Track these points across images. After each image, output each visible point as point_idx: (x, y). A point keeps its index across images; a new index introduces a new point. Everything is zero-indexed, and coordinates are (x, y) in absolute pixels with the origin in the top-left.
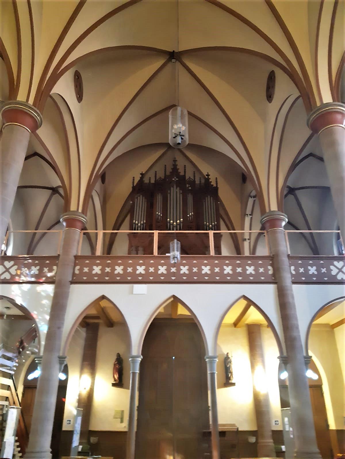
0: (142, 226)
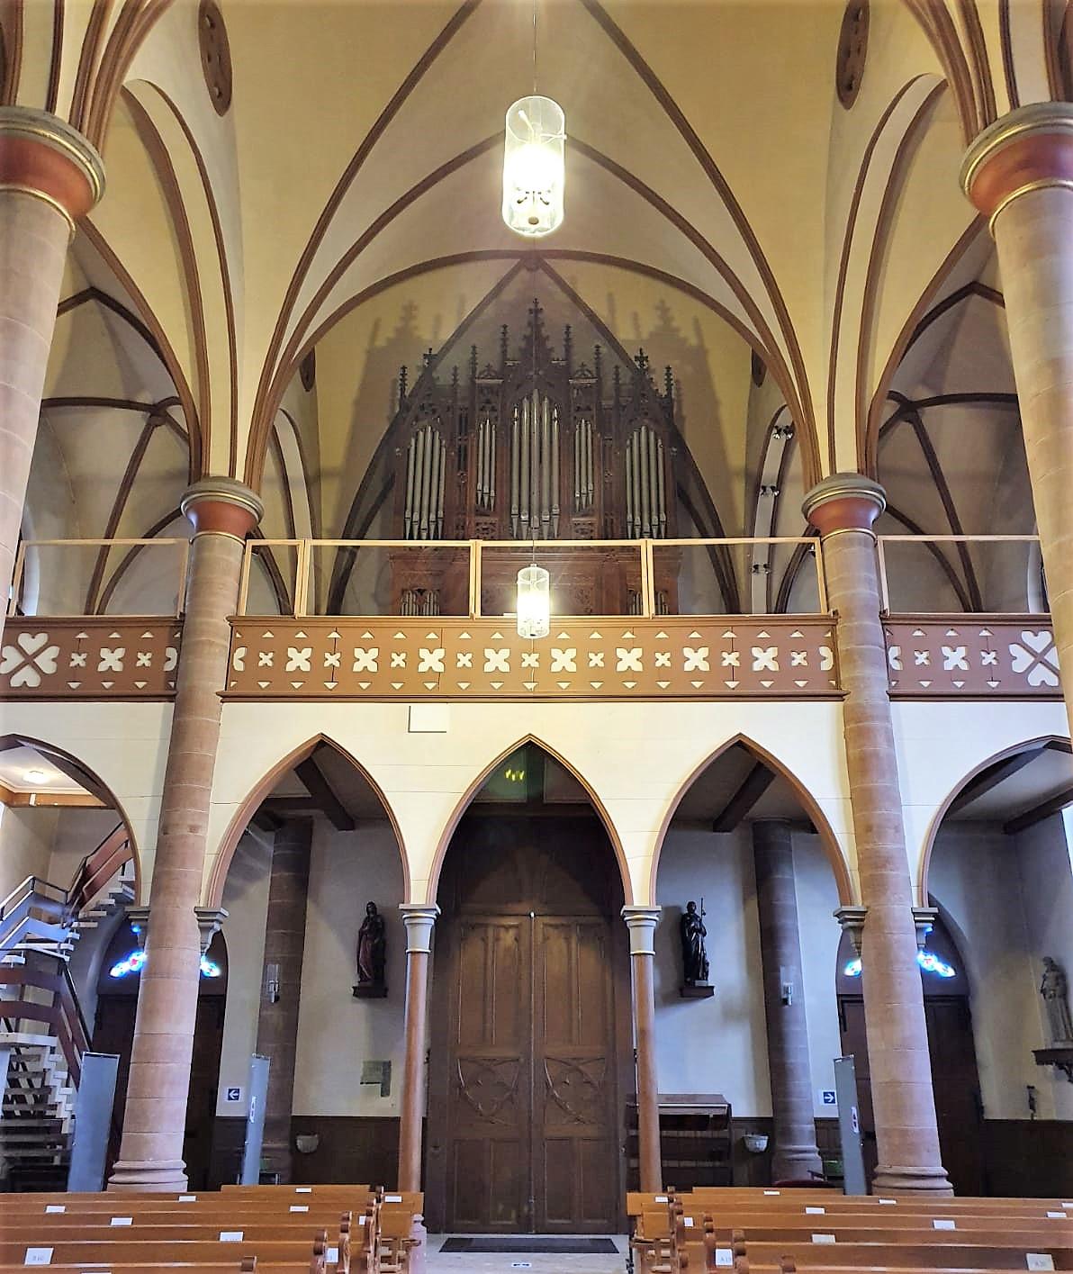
0: (432, 527)
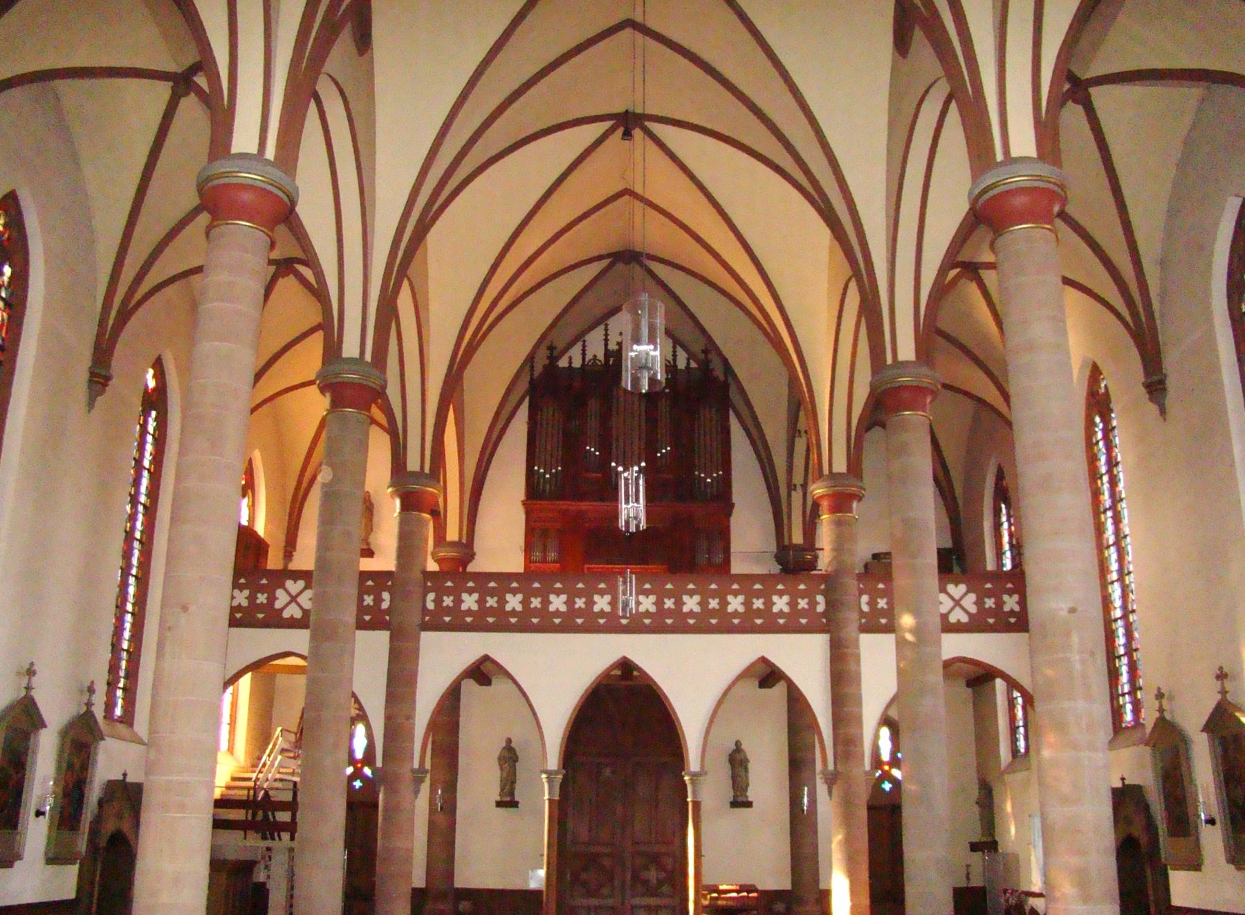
0: (554, 480)
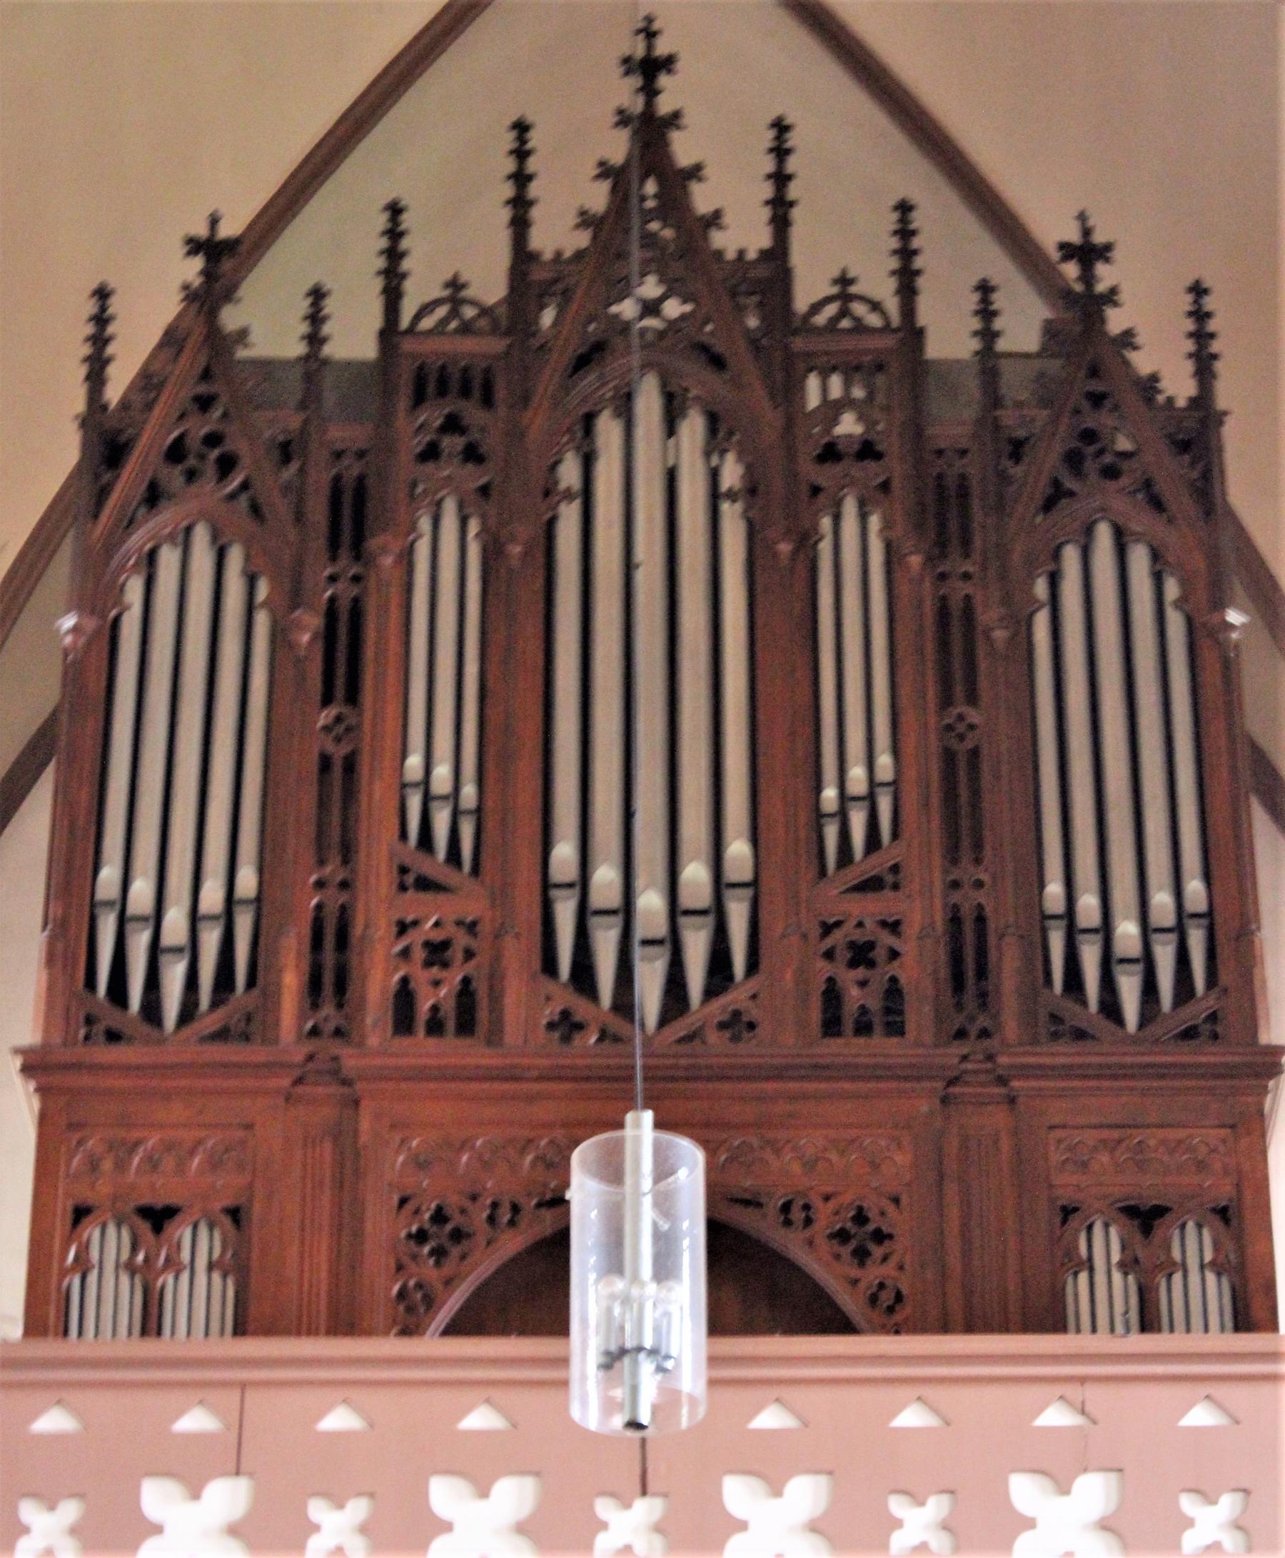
0: (211, 940)
